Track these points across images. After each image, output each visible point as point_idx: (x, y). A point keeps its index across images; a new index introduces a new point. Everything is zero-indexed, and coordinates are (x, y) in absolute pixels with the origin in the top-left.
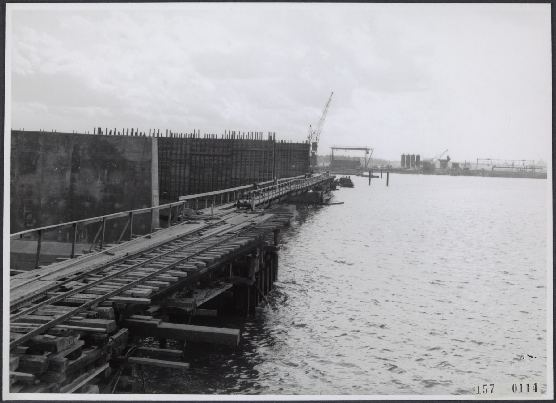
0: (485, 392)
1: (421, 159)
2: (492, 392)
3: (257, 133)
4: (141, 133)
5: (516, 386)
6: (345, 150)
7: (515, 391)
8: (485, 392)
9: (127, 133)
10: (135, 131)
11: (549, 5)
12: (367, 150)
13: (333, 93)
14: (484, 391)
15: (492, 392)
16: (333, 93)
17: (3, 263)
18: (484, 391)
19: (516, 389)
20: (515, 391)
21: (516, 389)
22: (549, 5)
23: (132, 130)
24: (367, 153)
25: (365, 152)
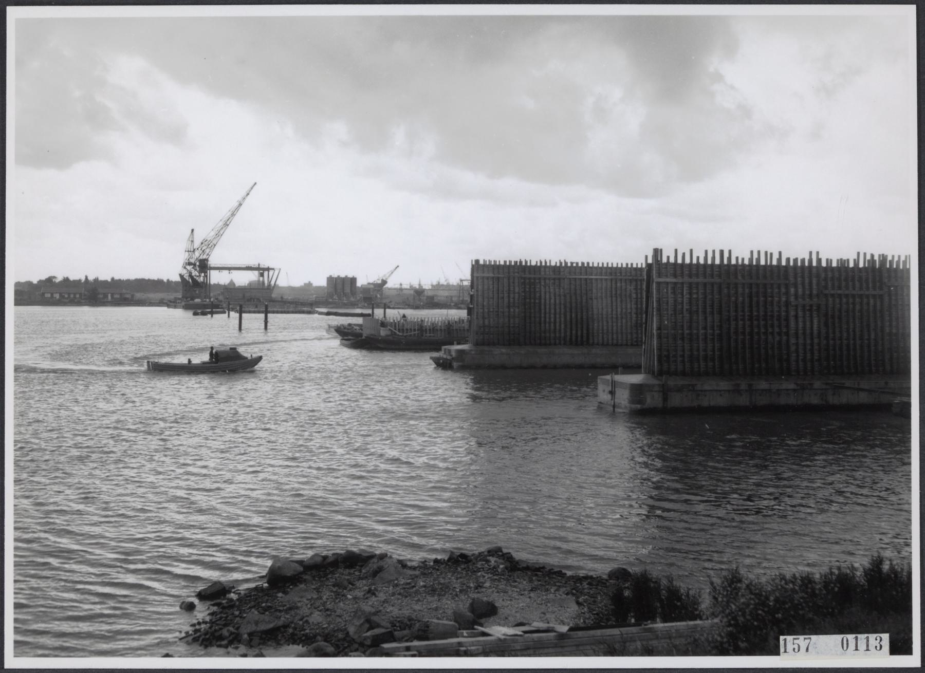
0: (796, 650)
1: (359, 284)
2: (807, 650)
3: (771, 254)
4: (788, 260)
5: (847, 641)
6: (227, 272)
7: (845, 648)
8: (796, 650)
9: (714, 258)
10: (726, 255)
11: (914, 7)
12: (262, 270)
13: (255, 184)
14: (794, 649)
15: (807, 650)
16: (255, 184)
17: (844, 668)
18: (794, 649)
19: (847, 644)
20: (845, 648)
21: (847, 644)
22: (914, 7)
23: (722, 252)
24: (262, 275)
25: (256, 273)
